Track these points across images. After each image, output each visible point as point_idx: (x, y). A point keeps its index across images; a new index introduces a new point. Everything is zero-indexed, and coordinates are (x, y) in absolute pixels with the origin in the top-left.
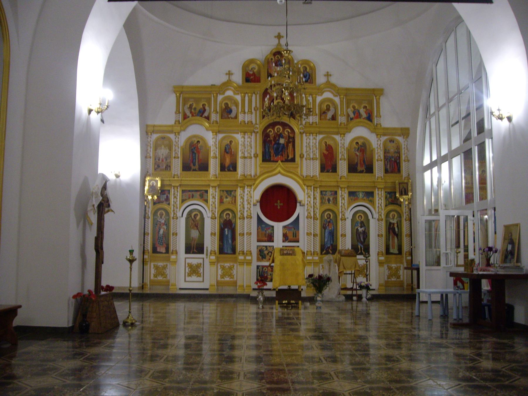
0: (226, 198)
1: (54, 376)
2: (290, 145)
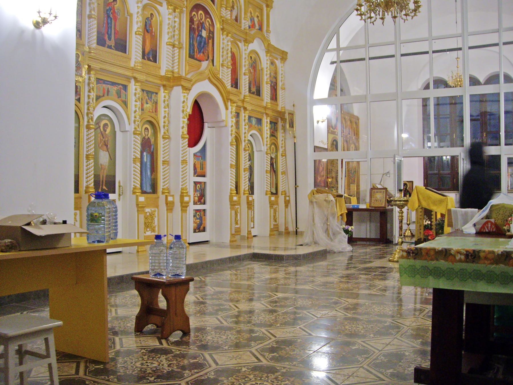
0: (147, 103)
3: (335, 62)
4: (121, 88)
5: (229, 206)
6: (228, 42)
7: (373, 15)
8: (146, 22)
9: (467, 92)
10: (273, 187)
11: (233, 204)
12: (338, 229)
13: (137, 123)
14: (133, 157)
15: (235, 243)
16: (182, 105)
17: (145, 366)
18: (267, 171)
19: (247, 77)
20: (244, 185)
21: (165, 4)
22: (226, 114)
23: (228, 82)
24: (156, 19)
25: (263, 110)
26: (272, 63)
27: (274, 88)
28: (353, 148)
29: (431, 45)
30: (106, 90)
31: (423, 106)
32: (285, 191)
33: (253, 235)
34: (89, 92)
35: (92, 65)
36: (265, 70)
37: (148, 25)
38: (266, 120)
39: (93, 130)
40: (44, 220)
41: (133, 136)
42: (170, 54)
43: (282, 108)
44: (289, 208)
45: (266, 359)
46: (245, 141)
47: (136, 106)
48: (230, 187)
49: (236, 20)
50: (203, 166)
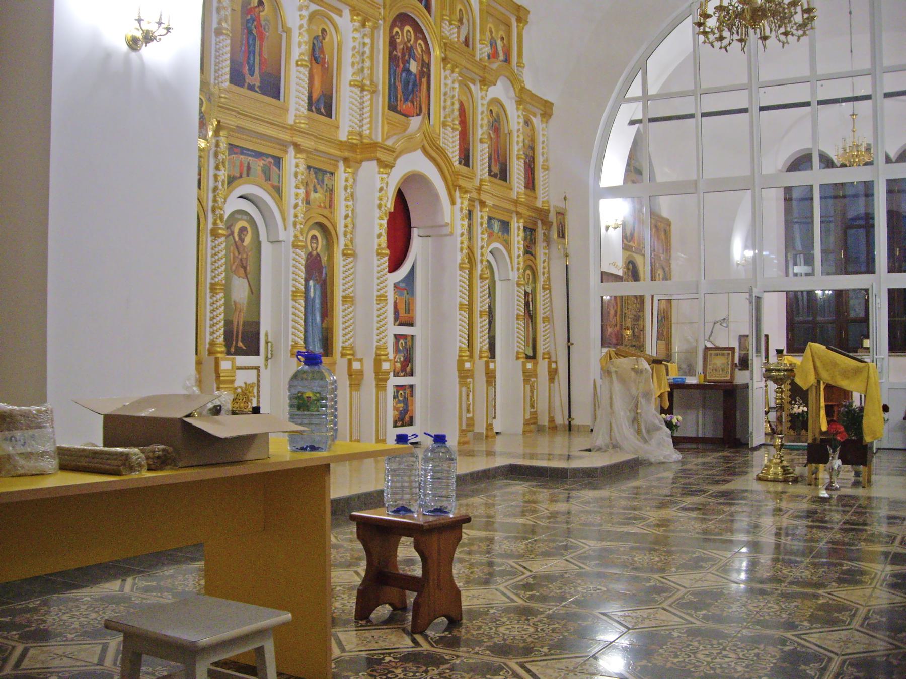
1: (652, 519)
2: (424, 80)
3: (639, 121)
4: (270, 163)
5: (458, 380)
6: (453, 83)
7: (726, 33)
9: (880, 178)
11: (464, 376)
12: (657, 422)
13: (298, 226)
14: (291, 288)
15: (466, 447)
16: (378, 194)
18: (518, 316)
19: (486, 146)
20: (481, 342)
21: (346, 12)
22: (451, 213)
23: (453, 153)
24: (332, 37)
25: (511, 207)
26: (527, 122)
27: (530, 166)
28: (661, 276)
29: (814, 92)
30: (246, 165)
31: (785, 199)
32: (549, 353)
33: (495, 431)
34: (217, 168)
35: (222, 120)
36: (515, 134)
38: (516, 225)
39: (223, 239)
40: (215, 407)
41: (291, 250)
42: (356, 102)
43: (543, 202)
44: (556, 381)
45: (429, 642)
46: (482, 262)
47: (297, 195)
48: (458, 344)
49: (466, 42)
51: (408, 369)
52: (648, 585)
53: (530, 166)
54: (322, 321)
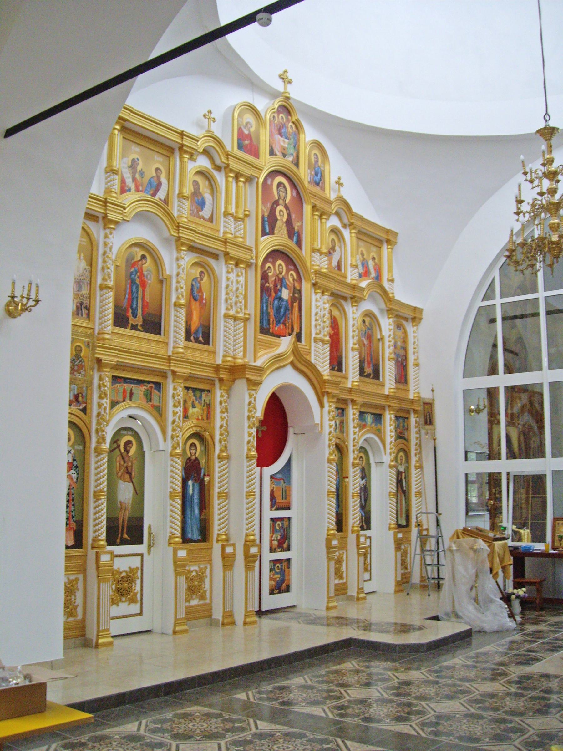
0: (194, 407)
2: (296, 305)
4: (151, 387)
8: (192, 285)
10: (401, 517)
14: (170, 490)
17: (285, 745)
22: (322, 415)
27: (402, 364)
30: (129, 391)
36: (387, 340)
37: (195, 290)
41: (169, 458)
50: (286, 494)
51: (285, 545)
52: (510, 726)
53: (402, 364)
54: (201, 513)
